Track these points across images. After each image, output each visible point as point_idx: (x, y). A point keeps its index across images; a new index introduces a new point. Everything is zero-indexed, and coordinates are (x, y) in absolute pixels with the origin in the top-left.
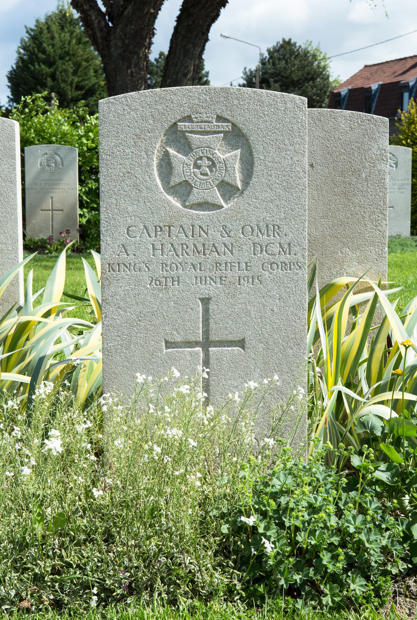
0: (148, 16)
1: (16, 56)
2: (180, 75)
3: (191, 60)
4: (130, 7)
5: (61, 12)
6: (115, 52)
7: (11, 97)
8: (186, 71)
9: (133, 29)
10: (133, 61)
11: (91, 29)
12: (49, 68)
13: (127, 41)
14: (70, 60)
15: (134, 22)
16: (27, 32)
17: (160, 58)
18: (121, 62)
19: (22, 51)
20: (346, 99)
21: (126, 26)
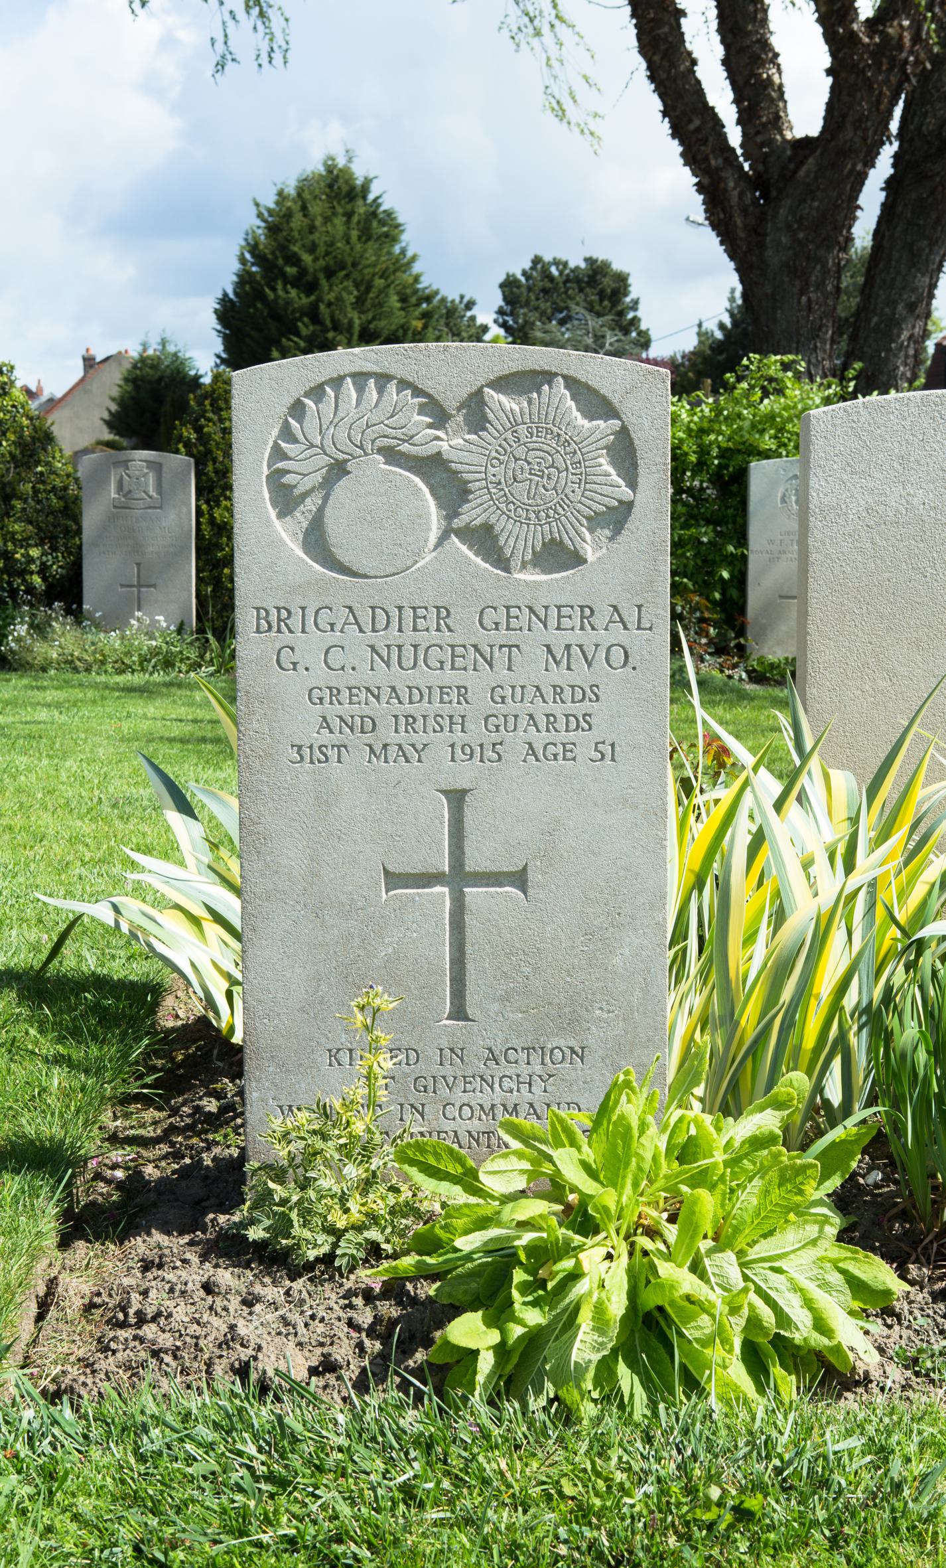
0: (852, 178)
1: (236, 266)
2: (900, 307)
3: (923, 275)
4: (811, 160)
5: (330, 170)
6: (774, 258)
7: (224, 356)
8: (913, 299)
9: (818, 209)
10: (813, 278)
11: (724, 210)
12: (308, 296)
13: (801, 235)
14: (347, 276)
15: (819, 194)
16: (260, 215)
17: (532, 268)
18: (786, 279)
19: (248, 256)
21: (802, 201)
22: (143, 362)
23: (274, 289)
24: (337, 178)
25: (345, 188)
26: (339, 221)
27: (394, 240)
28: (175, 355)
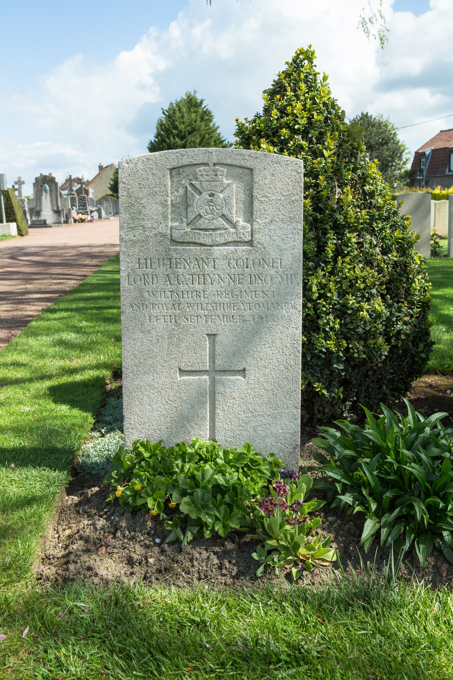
5: (188, 97)
16: (164, 113)
23: (169, 139)
24: (191, 100)
25: (194, 103)
27: (211, 121)
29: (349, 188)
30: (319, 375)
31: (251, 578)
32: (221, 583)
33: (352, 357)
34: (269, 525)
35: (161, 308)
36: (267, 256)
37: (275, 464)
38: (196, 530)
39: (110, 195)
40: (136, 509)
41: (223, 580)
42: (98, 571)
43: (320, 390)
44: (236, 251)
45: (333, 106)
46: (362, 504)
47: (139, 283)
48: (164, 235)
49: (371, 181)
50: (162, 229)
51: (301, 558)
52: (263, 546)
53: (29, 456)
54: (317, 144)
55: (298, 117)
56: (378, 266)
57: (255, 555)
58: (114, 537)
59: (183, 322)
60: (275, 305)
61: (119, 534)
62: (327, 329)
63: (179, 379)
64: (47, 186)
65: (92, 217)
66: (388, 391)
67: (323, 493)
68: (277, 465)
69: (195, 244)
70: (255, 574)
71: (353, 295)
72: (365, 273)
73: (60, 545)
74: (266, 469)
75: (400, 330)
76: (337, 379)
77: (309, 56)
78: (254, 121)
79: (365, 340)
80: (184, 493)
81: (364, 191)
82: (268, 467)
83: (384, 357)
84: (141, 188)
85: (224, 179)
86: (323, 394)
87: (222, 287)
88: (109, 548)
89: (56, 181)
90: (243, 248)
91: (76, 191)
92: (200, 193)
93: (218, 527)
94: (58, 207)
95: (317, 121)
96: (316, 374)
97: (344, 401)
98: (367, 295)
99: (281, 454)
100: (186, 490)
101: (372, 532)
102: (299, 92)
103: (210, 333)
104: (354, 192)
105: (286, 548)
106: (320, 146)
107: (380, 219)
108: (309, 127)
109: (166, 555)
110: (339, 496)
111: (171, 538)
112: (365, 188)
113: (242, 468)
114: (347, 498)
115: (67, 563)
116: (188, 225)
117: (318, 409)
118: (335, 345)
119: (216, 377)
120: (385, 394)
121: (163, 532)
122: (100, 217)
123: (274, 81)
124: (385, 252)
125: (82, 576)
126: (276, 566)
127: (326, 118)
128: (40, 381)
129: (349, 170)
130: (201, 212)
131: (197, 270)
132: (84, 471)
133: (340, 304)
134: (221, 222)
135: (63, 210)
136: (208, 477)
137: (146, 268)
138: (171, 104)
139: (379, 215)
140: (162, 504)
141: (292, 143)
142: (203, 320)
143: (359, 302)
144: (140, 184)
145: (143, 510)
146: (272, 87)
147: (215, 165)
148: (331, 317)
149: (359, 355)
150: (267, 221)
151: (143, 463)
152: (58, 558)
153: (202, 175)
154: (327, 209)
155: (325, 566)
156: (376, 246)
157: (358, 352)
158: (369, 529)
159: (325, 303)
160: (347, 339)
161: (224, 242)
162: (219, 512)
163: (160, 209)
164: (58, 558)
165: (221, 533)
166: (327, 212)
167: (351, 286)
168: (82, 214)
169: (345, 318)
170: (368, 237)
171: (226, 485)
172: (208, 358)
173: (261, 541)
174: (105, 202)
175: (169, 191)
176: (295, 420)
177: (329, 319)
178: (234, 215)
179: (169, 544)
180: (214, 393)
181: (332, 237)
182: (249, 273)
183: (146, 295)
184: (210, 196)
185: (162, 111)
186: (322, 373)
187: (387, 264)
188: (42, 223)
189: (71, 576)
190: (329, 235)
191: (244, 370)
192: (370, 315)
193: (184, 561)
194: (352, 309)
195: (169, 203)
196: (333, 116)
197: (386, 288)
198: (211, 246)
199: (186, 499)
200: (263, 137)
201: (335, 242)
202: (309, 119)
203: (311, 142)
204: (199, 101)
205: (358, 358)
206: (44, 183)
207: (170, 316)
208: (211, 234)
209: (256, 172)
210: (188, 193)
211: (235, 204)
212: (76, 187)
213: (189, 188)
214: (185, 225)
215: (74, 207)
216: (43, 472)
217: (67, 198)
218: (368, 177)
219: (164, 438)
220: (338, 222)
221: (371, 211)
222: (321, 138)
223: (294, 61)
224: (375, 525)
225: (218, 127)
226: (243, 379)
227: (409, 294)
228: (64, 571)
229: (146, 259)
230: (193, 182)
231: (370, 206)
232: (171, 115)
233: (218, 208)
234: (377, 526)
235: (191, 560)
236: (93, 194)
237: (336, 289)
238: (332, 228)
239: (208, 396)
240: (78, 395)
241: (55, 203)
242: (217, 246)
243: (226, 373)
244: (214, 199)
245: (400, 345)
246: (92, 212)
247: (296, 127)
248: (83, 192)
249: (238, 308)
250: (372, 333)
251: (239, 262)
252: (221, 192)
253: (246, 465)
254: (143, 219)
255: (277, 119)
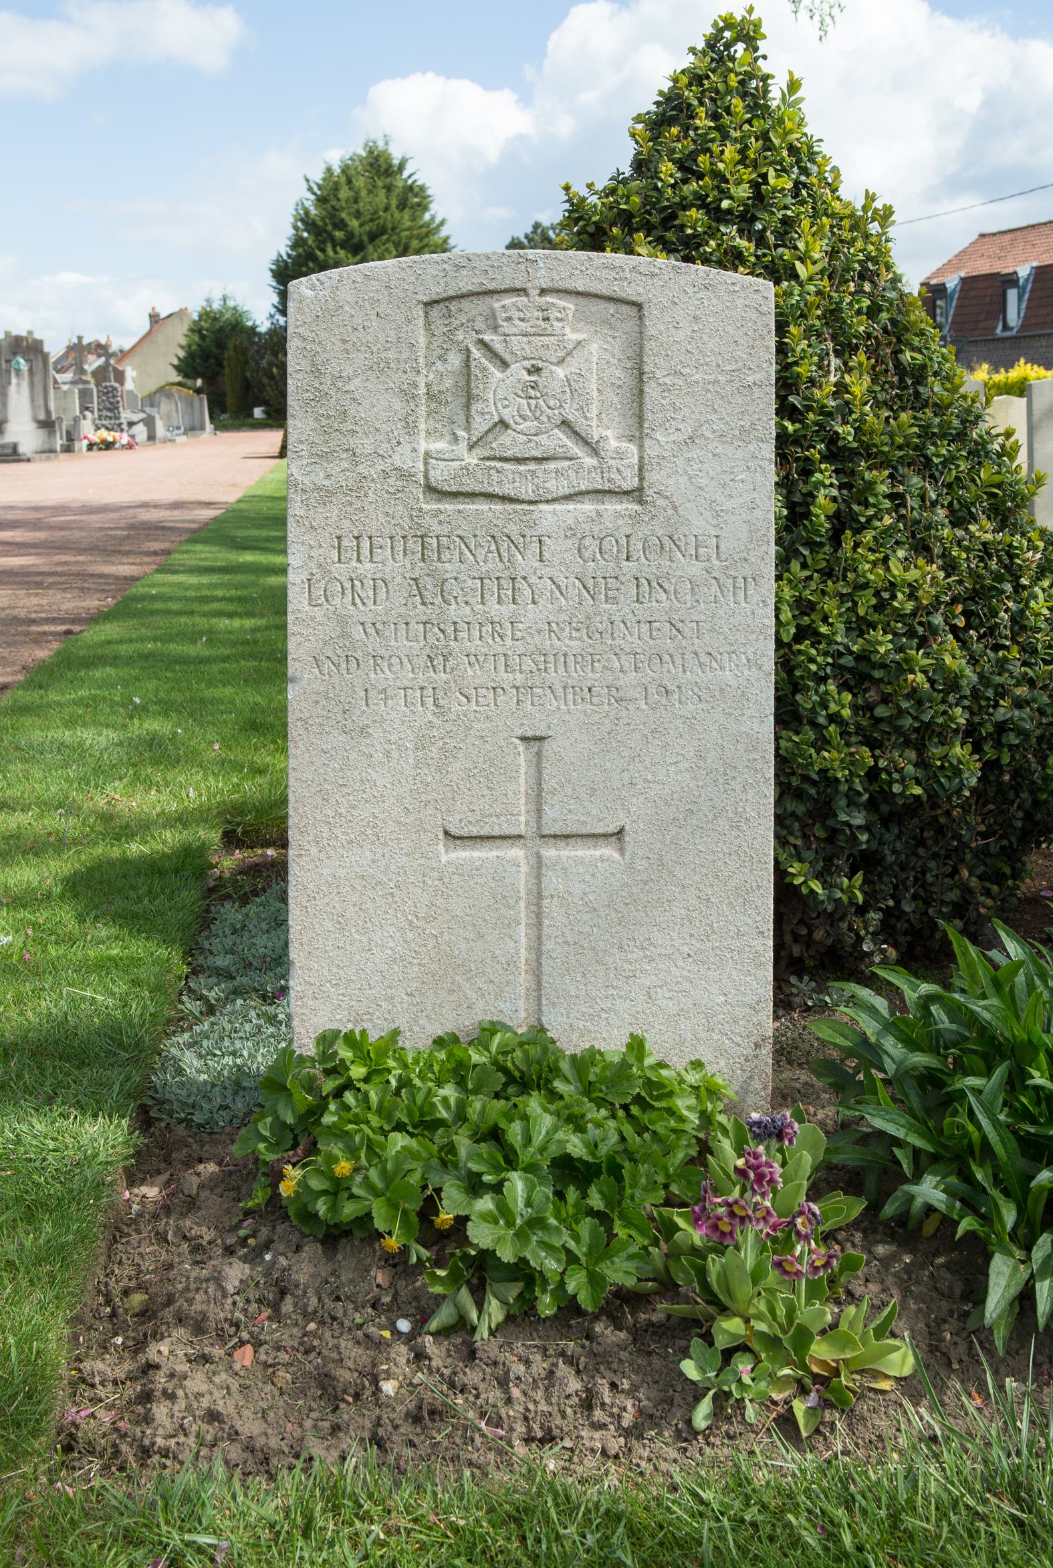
5: (371, 152)
14: (388, 240)
16: (310, 189)
17: (534, 232)
20: (1029, 288)
22: (206, 315)
23: (323, 251)
24: (377, 158)
25: (384, 167)
26: (382, 193)
27: (426, 209)
28: (235, 308)
29: (862, 357)
30: (799, 842)
31: (678, 1435)
32: (593, 1450)
33: (889, 796)
34: (724, 1275)
35: (396, 668)
36: (682, 529)
37: (708, 1090)
38: (513, 1291)
39: (179, 384)
40: (336, 1233)
41: (595, 1439)
42: (238, 1425)
43: (805, 882)
44: (599, 515)
45: (812, 156)
46: (970, 1206)
47: (337, 601)
48: (406, 476)
49: (916, 341)
50: (403, 458)
51: (815, 1369)
52: (708, 1339)
53: (19, 1076)
54: (776, 246)
55: (727, 182)
56: (943, 556)
57: (689, 1368)
58: (277, 1316)
59: (456, 705)
60: (704, 659)
61: (287, 1306)
62: (821, 720)
63: (444, 859)
64: (22, 361)
65: (132, 436)
66: (974, 882)
67: (860, 1173)
68: (713, 1093)
69: (490, 496)
70: (689, 1422)
71: (885, 632)
72: (913, 575)
73: (119, 1340)
74: (688, 1108)
75: (1005, 722)
76: (847, 852)
77: (748, 33)
78: (613, 191)
79: (920, 748)
80: (475, 1186)
81: (898, 365)
82: (692, 1101)
83: (967, 794)
84: (347, 351)
85: (567, 330)
86: (812, 891)
87: (560, 610)
88: (262, 1350)
89: (46, 349)
90: (619, 507)
91: (94, 374)
92: (505, 365)
93: (576, 1284)
94: (48, 412)
95: (775, 190)
96: (792, 840)
97: (862, 910)
98: (920, 630)
99: (722, 1063)
100: (479, 1175)
101: (1014, 1291)
102: (726, 120)
103: (529, 734)
104: (873, 368)
105: (772, 1342)
106: (787, 254)
107: (943, 436)
108: (754, 206)
109: (429, 1367)
110: (906, 1187)
111: (443, 1316)
112: (901, 356)
113: (625, 1107)
114: (930, 1191)
115: (146, 1397)
116: (471, 447)
117: (793, 932)
118: (842, 761)
119: (543, 852)
120: (967, 890)
121: (417, 1298)
122: (151, 437)
123: (661, 93)
124: (960, 518)
125: (192, 1440)
126: (747, 1397)
127: (797, 184)
128: (34, 860)
129: (859, 312)
130: (507, 415)
131: (492, 566)
132: (171, 1113)
133: (851, 653)
134: (562, 438)
135: (60, 419)
136: (538, 1139)
137: (359, 560)
138: (329, 170)
139: (940, 426)
140: (415, 1219)
141: (713, 243)
142: (508, 700)
143: (900, 649)
144: (344, 341)
145: (358, 1234)
146: (654, 108)
147: (543, 292)
148: (832, 687)
149: (905, 787)
150: (680, 437)
151: (349, 1097)
152: (115, 1382)
153: (509, 319)
154: (809, 408)
155: (883, 1392)
156: (934, 504)
157: (902, 781)
158: (1003, 1283)
159: (813, 652)
160: (872, 744)
161: (567, 491)
162: (576, 1238)
163: (397, 405)
164: (115, 1382)
165: (584, 1299)
166: (811, 416)
167: (879, 607)
168: (107, 428)
169: (866, 691)
170: (915, 480)
171: (590, 1159)
172: (523, 801)
173: (697, 1323)
174: (163, 399)
175: (421, 360)
176: (758, 967)
177: (827, 692)
178: (594, 423)
179: (440, 1334)
180: (540, 896)
181: (827, 482)
182: (634, 572)
183: (358, 633)
184: (529, 373)
185: (305, 185)
186: (805, 836)
187: (967, 550)
188: (9, 451)
189: (160, 1441)
190: (818, 475)
191: (620, 833)
192: (932, 682)
193: (482, 1386)
194: (884, 666)
195: (422, 390)
196: (815, 181)
197: (964, 613)
198: (531, 502)
199: (486, 1203)
200: (637, 230)
201: (835, 492)
202: (756, 186)
203: (761, 241)
204: (396, 162)
205: (902, 794)
206: (15, 354)
207: (422, 688)
208: (534, 472)
209: (650, 312)
210: (473, 364)
211: (595, 394)
212: (93, 363)
213: (476, 353)
214: (462, 447)
215: (87, 413)
216: (61, 1123)
217: (71, 391)
218: (907, 330)
219: (401, 1023)
220: (840, 443)
221: (920, 415)
222: (787, 233)
223: (711, 44)
224: (1015, 1269)
225: (442, 223)
226: (617, 856)
227: (1024, 628)
228: (137, 1423)
229: (357, 538)
230: (487, 338)
231: (918, 403)
232: (328, 194)
233: (552, 403)
234: (1024, 1273)
235: (503, 1383)
236: (134, 380)
237: (840, 615)
238: (825, 458)
239: (522, 904)
240: (140, 899)
241: (41, 402)
242: (547, 502)
243: (572, 841)
244: (541, 381)
245: (1006, 759)
246: (131, 424)
247: (725, 204)
248: (109, 375)
249: (605, 667)
250: (938, 730)
251: (606, 545)
252: (561, 362)
253: (638, 1099)
254: (353, 432)
255: (673, 186)
